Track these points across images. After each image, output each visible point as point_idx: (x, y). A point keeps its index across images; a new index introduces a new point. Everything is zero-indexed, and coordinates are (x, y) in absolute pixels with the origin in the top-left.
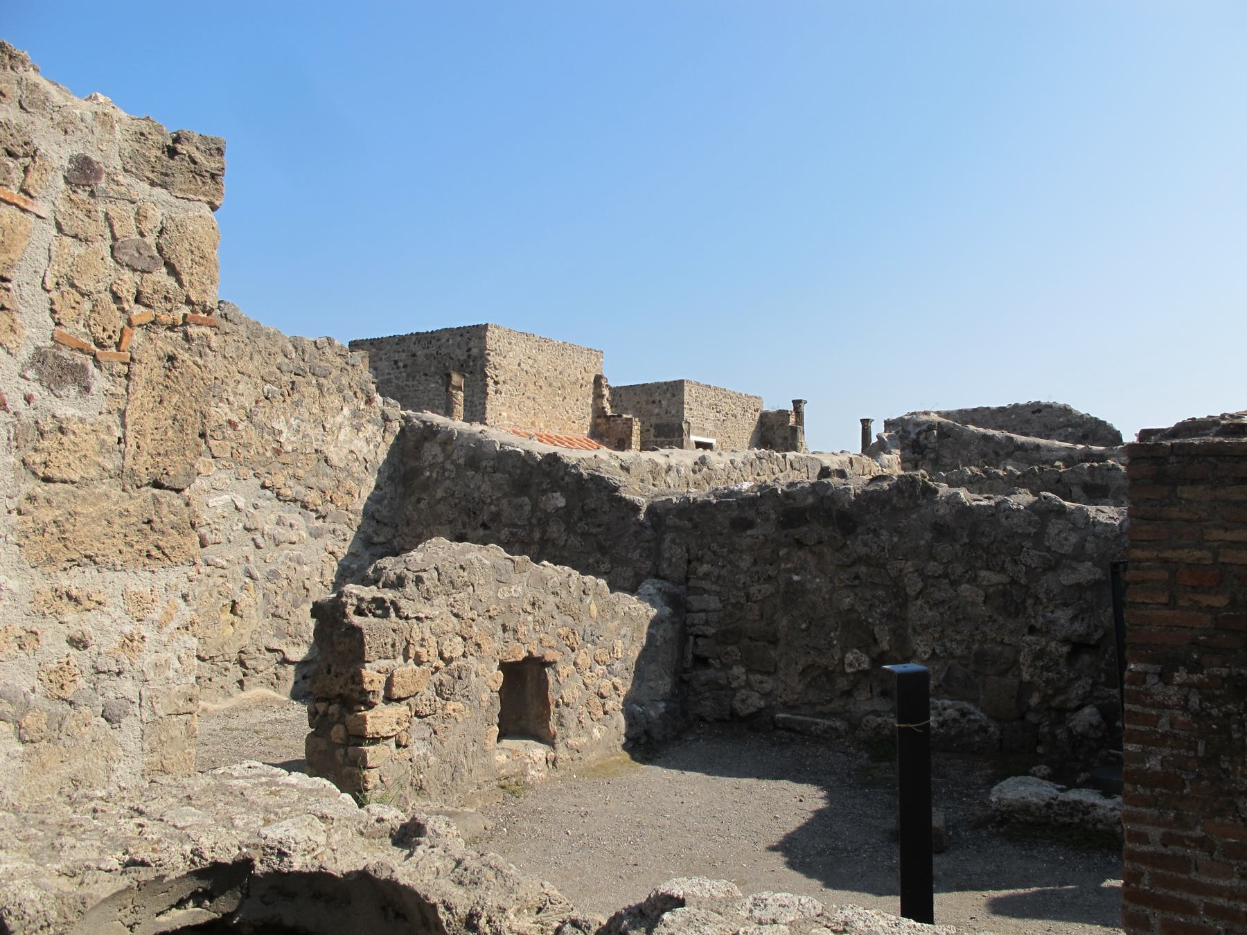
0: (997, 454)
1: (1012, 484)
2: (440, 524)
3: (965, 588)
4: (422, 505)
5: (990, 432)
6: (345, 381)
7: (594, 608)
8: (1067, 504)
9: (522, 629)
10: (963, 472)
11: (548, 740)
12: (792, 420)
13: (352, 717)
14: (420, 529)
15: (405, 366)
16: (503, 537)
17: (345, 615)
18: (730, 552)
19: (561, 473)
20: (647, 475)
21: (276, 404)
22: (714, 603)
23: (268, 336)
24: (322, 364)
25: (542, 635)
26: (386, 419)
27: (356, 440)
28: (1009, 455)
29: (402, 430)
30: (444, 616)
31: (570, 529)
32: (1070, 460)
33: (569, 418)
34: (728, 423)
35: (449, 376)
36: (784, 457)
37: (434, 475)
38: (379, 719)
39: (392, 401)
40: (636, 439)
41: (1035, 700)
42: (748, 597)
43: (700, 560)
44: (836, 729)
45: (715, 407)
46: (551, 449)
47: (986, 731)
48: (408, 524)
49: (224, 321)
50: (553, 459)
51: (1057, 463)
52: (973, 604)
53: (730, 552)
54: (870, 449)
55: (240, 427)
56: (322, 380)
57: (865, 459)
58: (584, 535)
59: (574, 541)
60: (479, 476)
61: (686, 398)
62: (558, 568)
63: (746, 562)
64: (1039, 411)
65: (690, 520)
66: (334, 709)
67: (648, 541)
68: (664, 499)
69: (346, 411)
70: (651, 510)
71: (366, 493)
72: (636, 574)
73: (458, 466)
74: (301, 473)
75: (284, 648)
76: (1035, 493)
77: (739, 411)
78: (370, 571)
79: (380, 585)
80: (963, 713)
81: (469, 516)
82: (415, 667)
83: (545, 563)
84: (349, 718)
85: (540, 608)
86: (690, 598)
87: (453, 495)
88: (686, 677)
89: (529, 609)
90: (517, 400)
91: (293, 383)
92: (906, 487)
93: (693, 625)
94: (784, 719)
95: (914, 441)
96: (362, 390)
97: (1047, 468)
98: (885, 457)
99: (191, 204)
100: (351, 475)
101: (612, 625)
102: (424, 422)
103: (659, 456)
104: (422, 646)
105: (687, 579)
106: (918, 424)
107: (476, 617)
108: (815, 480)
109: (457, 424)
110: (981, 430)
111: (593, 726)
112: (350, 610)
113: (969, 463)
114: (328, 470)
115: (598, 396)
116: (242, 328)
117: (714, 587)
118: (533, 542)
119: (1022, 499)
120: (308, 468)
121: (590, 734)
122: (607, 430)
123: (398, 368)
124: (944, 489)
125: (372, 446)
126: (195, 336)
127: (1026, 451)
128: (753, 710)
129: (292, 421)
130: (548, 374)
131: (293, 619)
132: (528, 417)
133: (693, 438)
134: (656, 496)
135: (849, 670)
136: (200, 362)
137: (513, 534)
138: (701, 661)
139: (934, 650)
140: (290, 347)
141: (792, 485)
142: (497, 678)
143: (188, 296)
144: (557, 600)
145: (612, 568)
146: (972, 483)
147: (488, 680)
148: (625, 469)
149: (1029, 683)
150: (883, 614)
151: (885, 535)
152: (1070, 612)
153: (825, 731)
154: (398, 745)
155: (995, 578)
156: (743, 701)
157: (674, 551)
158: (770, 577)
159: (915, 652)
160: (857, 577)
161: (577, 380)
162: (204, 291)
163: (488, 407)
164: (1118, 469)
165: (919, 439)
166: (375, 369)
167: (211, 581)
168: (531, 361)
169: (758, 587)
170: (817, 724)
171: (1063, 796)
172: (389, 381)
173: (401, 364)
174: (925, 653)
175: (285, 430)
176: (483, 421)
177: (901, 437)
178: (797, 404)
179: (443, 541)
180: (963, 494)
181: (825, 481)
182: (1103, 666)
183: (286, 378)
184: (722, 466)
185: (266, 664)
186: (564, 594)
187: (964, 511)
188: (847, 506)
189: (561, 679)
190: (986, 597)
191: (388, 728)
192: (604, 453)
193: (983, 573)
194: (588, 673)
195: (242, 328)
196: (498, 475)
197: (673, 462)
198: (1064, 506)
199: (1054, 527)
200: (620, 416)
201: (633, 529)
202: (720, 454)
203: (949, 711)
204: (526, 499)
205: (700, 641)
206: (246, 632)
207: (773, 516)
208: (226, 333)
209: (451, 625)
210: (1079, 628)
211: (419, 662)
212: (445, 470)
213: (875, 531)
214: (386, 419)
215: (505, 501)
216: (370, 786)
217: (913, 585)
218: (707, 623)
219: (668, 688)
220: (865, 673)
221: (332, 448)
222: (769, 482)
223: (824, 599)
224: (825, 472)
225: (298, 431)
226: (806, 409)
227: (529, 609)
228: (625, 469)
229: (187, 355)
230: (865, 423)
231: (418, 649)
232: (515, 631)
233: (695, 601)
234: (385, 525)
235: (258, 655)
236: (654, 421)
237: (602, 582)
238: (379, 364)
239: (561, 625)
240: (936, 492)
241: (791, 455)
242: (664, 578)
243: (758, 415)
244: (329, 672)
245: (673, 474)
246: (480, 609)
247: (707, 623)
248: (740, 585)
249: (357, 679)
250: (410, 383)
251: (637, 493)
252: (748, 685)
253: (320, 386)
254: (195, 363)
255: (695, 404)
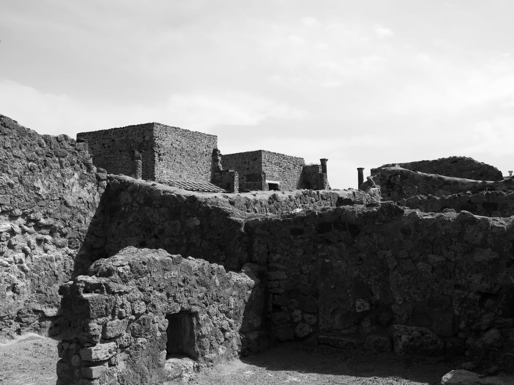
0: (434, 187)
1: (444, 206)
3: (421, 265)
4: (121, 227)
5: (430, 175)
7: (217, 281)
9: (178, 295)
13: (83, 351)
15: (109, 147)
16: (166, 242)
17: (78, 293)
20: (243, 205)
22: (283, 276)
23: (30, 135)
24: (61, 150)
25: (189, 298)
26: (99, 179)
27: (82, 193)
28: (440, 187)
30: (135, 290)
32: (476, 189)
33: (200, 173)
35: (133, 152)
37: (127, 209)
38: (100, 351)
39: (102, 169)
40: (236, 188)
41: (462, 325)
42: (301, 272)
43: (275, 252)
44: (352, 343)
45: (278, 164)
46: (192, 193)
47: (436, 343)
50: (193, 199)
51: (468, 192)
54: (363, 186)
56: (62, 159)
57: (362, 192)
61: (263, 160)
62: (197, 260)
63: (299, 253)
65: (268, 230)
66: (73, 346)
68: (253, 219)
69: (76, 176)
71: (88, 220)
74: (51, 211)
75: (44, 310)
76: (457, 212)
77: (291, 166)
78: (92, 267)
79: (98, 274)
80: (423, 334)
82: (119, 320)
83: (190, 257)
84: (82, 352)
85: (188, 283)
86: (270, 273)
89: (182, 284)
90: (171, 164)
92: (387, 209)
93: (272, 288)
96: (85, 164)
97: (461, 194)
98: (372, 189)
100: (80, 211)
101: (228, 290)
102: (120, 180)
103: (249, 195)
105: (268, 262)
107: (152, 290)
109: (140, 181)
111: (219, 347)
112: (81, 290)
113: (419, 193)
114: (67, 209)
117: (282, 267)
118: (182, 247)
120: (55, 208)
121: (217, 351)
123: (105, 148)
124: (407, 211)
125: (91, 194)
127: (450, 185)
128: (306, 334)
129: (45, 182)
130: (187, 149)
131: (49, 293)
132: (176, 178)
134: (250, 217)
135: (358, 311)
137: (172, 241)
138: (277, 308)
139: (405, 299)
140: (43, 141)
141: (323, 210)
144: (197, 278)
145: (226, 258)
146: (426, 207)
147: (160, 323)
148: (232, 203)
152: (480, 276)
155: (437, 259)
156: (301, 329)
158: (313, 260)
160: (361, 259)
161: (204, 152)
164: (503, 194)
165: (389, 179)
166: (92, 149)
168: (178, 143)
170: (342, 341)
173: (106, 146)
175: (41, 187)
176: (154, 179)
177: (380, 179)
178: (323, 161)
179: (134, 249)
182: (500, 306)
184: (284, 199)
185: (34, 320)
186: (201, 274)
189: (200, 322)
190: (433, 268)
192: (220, 195)
193: (430, 256)
194: (215, 318)
195: (14, 131)
196: (162, 209)
197: (258, 197)
198: (475, 218)
202: (283, 193)
203: (414, 332)
204: (178, 221)
205: (276, 297)
206: (22, 302)
208: (5, 134)
209: (138, 295)
210: (486, 285)
212: (133, 207)
213: (370, 234)
214: (99, 179)
215: (166, 223)
218: (279, 287)
220: (367, 312)
221: (69, 197)
224: (341, 201)
225: (49, 188)
226: (328, 164)
227: (182, 284)
228: (232, 203)
231: (121, 310)
232: (174, 297)
233: (273, 275)
234: (100, 238)
235: (28, 314)
236: (246, 172)
238: (94, 146)
239: (200, 291)
240: (403, 212)
241: (321, 192)
242: (255, 262)
243: (302, 168)
244: (70, 325)
245: (258, 205)
246: (154, 285)
247: (279, 287)
248: (297, 265)
249: (86, 329)
250: (112, 156)
251: (239, 216)
252: (303, 321)
253: (61, 163)
255: (268, 163)
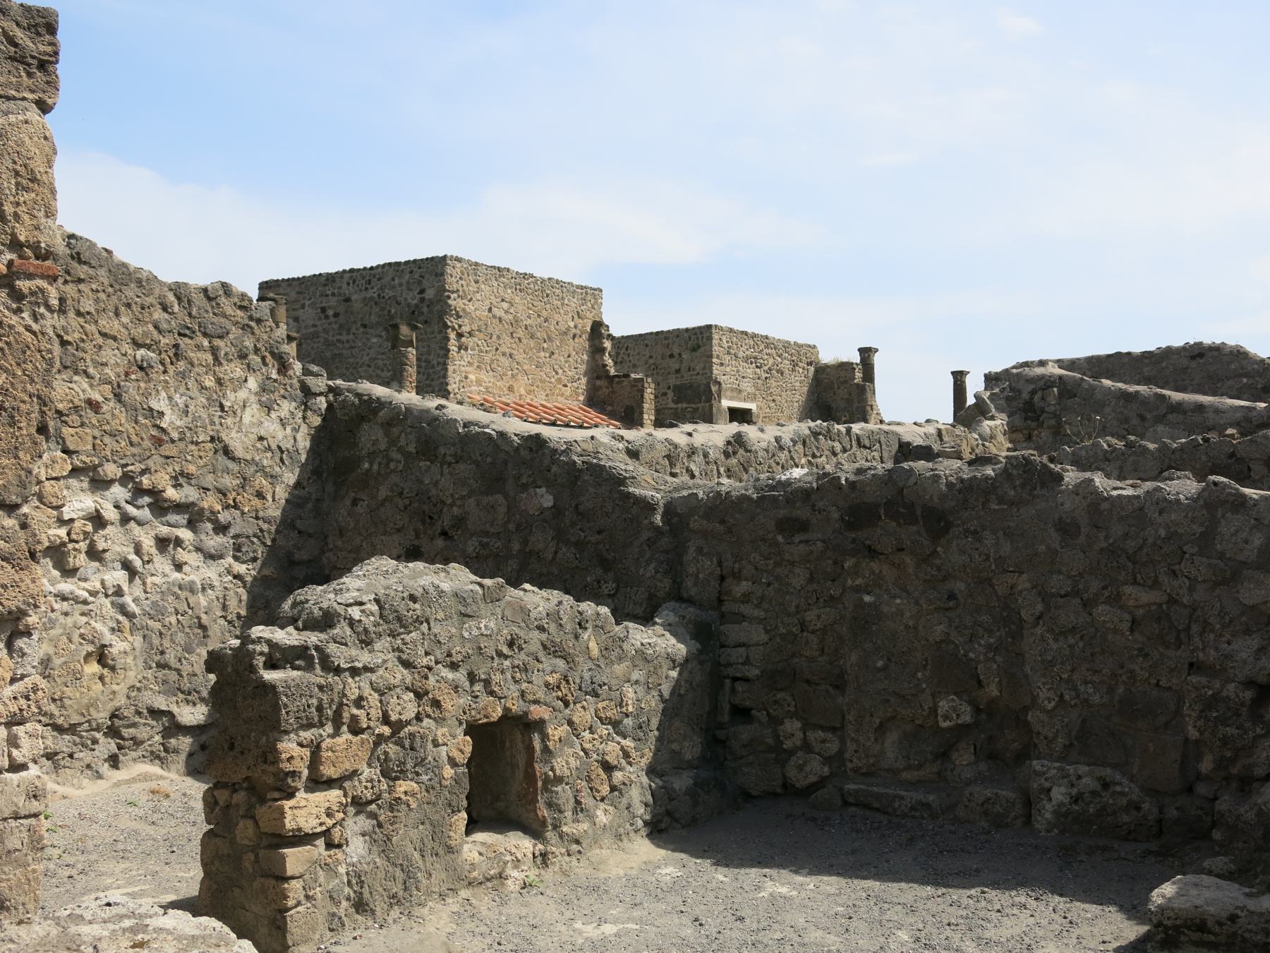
1: (1168, 464)
2: (385, 533)
4: (361, 508)
5: (1133, 388)
6: (249, 343)
7: (593, 645)
8: (1247, 491)
9: (497, 677)
10: (1097, 445)
11: (535, 830)
12: (858, 375)
13: (264, 809)
14: (358, 541)
15: (336, 315)
17: (252, 669)
18: (777, 564)
19: (547, 462)
20: (659, 459)
21: (154, 376)
22: (757, 634)
25: (524, 685)
26: (307, 392)
28: (1160, 419)
29: (330, 406)
30: (390, 665)
31: (560, 537)
33: (559, 380)
34: (772, 382)
35: (396, 327)
36: (849, 431)
37: (375, 467)
39: (315, 368)
40: (649, 417)
41: (1206, 765)
42: (803, 626)
43: (737, 576)
45: (752, 360)
47: (1138, 809)
48: (341, 535)
49: (75, 264)
50: (537, 442)
51: (1230, 431)
52: (1116, 631)
53: (777, 564)
54: (966, 414)
55: (105, 408)
56: (217, 342)
57: (960, 430)
58: (580, 545)
59: (567, 553)
60: (435, 469)
62: (544, 593)
63: (799, 578)
64: (1201, 355)
65: (722, 522)
67: (667, 552)
68: (685, 493)
70: (670, 509)
71: (282, 493)
72: (651, 597)
73: (407, 455)
74: (192, 469)
75: (174, 709)
76: (1200, 477)
78: (286, 606)
79: (300, 624)
81: (424, 522)
82: (350, 736)
83: (527, 586)
84: (261, 811)
85: (521, 649)
87: (401, 494)
88: (721, 734)
89: (505, 650)
90: (487, 358)
91: (176, 346)
92: (1020, 471)
94: (857, 791)
95: (1026, 403)
96: (272, 354)
97: (1213, 437)
99: (11, 104)
101: (619, 669)
102: (358, 395)
103: (677, 435)
104: (359, 707)
105: (720, 601)
106: (1030, 380)
107: (433, 664)
108: (889, 465)
109: (407, 397)
110: (1120, 385)
112: (260, 661)
113: (1104, 431)
114: (231, 465)
115: (596, 350)
116: (102, 272)
117: (756, 613)
119: (1184, 486)
120: (201, 462)
121: (591, 818)
122: (611, 395)
123: (327, 317)
124: (1072, 476)
126: (26, 291)
127: (1185, 413)
129: (177, 397)
130: (529, 322)
132: (497, 391)
133: (726, 403)
134: (676, 489)
136: (35, 327)
138: (742, 713)
139: (1061, 696)
140: (171, 297)
141: (859, 471)
142: (459, 745)
143: (14, 235)
144: (544, 636)
146: (1119, 466)
148: (633, 454)
149: (1197, 742)
150: (989, 647)
151: (989, 539)
152: (1254, 642)
153: (913, 808)
154: (330, 845)
155: (1147, 597)
157: (700, 568)
158: (832, 597)
159: (1034, 699)
160: (952, 596)
161: (568, 329)
162: (37, 228)
163: (451, 368)
165: (1031, 399)
166: (296, 319)
167: (69, 620)
168: (505, 305)
169: (816, 612)
170: (902, 798)
171: (1252, 904)
172: (315, 335)
173: (330, 313)
174: (1049, 700)
175: (168, 411)
177: (1008, 399)
178: (867, 354)
180: (1099, 480)
181: (905, 465)
183: (165, 341)
184: (764, 445)
185: (150, 733)
186: (552, 628)
187: (1095, 502)
188: (936, 500)
189: (550, 744)
190: (1133, 622)
191: (315, 822)
193: (1128, 589)
194: (587, 735)
195: (102, 272)
196: (462, 466)
197: (698, 440)
198: (1244, 496)
199: (1230, 525)
200: (627, 376)
201: (646, 535)
202: (762, 430)
205: (740, 687)
206: (121, 689)
207: (836, 515)
208: (80, 281)
209: (399, 676)
211: (356, 730)
213: (975, 532)
214: (307, 392)
215: (472, 501)
216: (290, 903)
217: (1030, 607)
218: (747, 662)
219: (697, 750)
222: (829, 468)
223: (907, 627)
224: (906, 451)
226: (878, 361)
227: (505, 650)
228: (633, 454)
229: (15, 318)
230: (959, 378)
231: (355, 711)
232: (487, 683)
233: (734, 632)
234: (310, 536)
235: (137, 719)
236: (673, 381)
237: (604, 610)
238: (300, 312)
240: (1059, 478)
241: (857, 428)
242: (690, 601)
243: (812, 369)
244: (232, 747)
245: (699, 458)
246: (438, 653)
247: (747, 662)
248: (792, 609)
249: (270, 757)
250: (344, 338)
251: (650, 485)
252: (806, 746)
253: (214, 351)
254: (28, 328)
255: (728, 357)
